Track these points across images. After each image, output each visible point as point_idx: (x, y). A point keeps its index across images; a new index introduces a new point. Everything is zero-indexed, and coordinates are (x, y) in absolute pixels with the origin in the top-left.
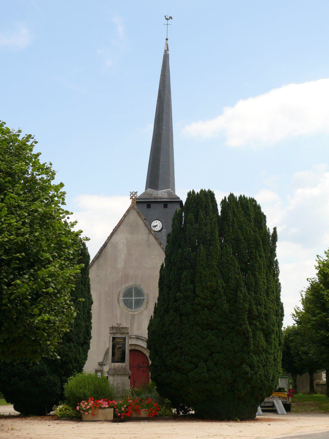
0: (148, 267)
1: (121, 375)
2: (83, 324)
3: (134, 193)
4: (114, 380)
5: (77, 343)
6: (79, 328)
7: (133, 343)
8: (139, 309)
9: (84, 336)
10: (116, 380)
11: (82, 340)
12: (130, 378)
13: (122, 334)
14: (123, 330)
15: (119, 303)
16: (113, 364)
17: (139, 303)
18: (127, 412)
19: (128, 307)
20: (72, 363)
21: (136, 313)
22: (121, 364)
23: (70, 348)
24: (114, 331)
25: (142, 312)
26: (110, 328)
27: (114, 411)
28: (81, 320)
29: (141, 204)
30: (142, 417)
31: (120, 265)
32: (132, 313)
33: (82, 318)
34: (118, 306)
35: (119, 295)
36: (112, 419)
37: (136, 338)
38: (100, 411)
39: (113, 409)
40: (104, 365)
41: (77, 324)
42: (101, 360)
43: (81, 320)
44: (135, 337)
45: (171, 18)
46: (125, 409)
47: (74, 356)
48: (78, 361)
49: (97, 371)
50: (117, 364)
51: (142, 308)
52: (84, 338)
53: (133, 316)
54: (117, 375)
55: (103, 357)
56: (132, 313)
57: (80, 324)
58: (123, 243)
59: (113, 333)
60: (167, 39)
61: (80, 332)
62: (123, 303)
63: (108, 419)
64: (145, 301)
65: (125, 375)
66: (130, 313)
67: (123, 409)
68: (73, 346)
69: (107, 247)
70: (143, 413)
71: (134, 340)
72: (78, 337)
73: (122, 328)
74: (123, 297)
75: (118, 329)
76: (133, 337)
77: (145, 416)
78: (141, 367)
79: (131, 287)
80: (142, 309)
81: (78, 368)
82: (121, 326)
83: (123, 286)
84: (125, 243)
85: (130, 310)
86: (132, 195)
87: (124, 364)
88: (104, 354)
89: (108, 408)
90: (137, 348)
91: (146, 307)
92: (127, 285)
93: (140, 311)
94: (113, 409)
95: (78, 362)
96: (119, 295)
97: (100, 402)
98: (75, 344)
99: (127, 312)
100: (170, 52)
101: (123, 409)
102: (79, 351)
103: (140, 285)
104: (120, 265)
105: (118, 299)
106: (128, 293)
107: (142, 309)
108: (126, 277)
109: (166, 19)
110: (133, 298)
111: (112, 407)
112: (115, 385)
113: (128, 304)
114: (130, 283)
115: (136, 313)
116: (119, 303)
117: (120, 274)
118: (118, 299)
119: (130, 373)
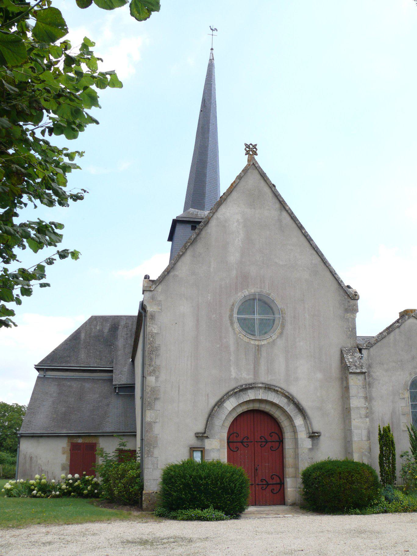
0: (281, 263)
3: (247, 149)
15: (232, 323)
21: (263, 343)
25: (274, 341)
29: (183, 225)
31: (234, 257)
32: (257, 343)
34: (230, 329)
35: (232, 310)
37: (265, 388)
40: (207, 437)
42: (200, 428)
44: (264, 386)
45: (216, 29)
49: (192, 449)
53: (259, 348)
55: (205, 422)
56: (257, 343)
58: (238, 221)
60: (212, 49)
66: (252, 342)
69: (209, 225)
71: (261, 391)
76: (260, 385)
79: (252, 297)
83: (239, 294)
84: (241, 221)
86: (251, 146)
88: (206, 416)
90: (257, 406)
91: (281, 333)
92: (246, 293)
93: (271, 340)
96: (232, 310)
100: (216, 62)
103: (269, 294)
104: (234, 257)
105: (231, 316)
106: (248, 304)
108: (244, 279)
109: (211, 29)
110: (257, 316)
113: (248, 327)
116: (232, 323)
117: (234, 273)
118: (231, 316)
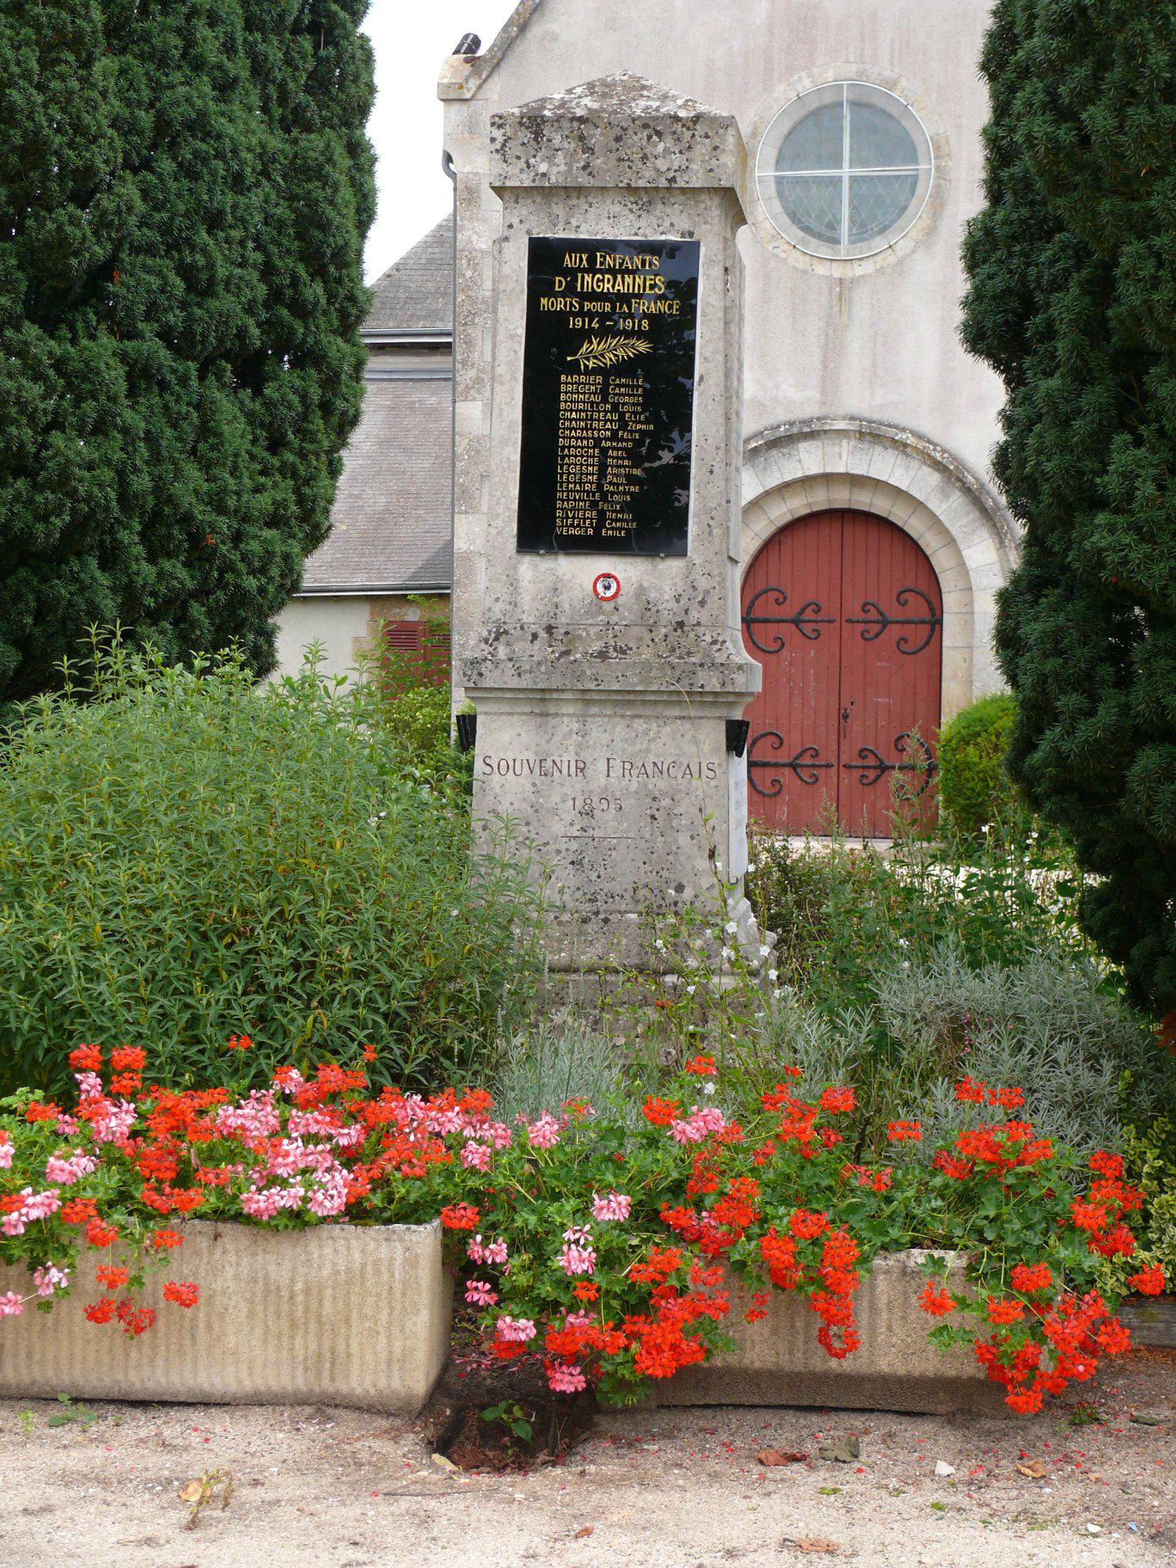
1: (628, 701)
2: (247, 128)
4: (543, 768)
5: (180, 342)
6: (188, 171)
7: (842, 470)
8: (879, 243)
9: (268, 271)
10: (567, 757)
11: (236, 307)
12: (736, 737)
13: (644, 197)
14: (665, 159)
16: (536, 571)
17: (879, 211)
18: (637, 1305)
19: (807, 230)
20: (111, 558)
21: (858, 270)
22: (629, 571)
23: (77, 380)
24: (554, 169)
26: (499, 122)
27: (459, 1267)
28: (225, 87)
30: (887, 1383)
32: (837, 271)
33: (239, 67)
36: (417, 1378)
37: (861, 435)
38: (225, 1268)
39: (424, 1239)
41: (162, 125)
43: (225, 87)
44: (854, 426)
46: (608, 1259)
47: (142, 482)
48: (195, 539)
50: (580, 573)
51: (903, 240)
52: (275, 296)
53: (843, 290)
54: (586, 698)
56: (837, 271)
57: (199, 126)
59: (544, 193)
61: (214, 221)
62: (777, 206)
63: (362, 1380)
64: (925, 189)
65: (684, 700)
66: (821, 269)
67: (576, 1259)
68: (115, 376)
70: (900, 1317)
71: (846, 446)
72: (185, 271)
73: (653, 126)
74: (779, 162)
75: (597, 137)
76: (841, 425)
77: (929, 1362)
78: (885, 623)
79: (828, 99)
80: (904, 247)
81: (197, 610)
82: (638, 108)
85: (825, 251)
87: (673, 566)
89: (356, 1213)
90: (863, 500)
92: (805, 85)
93: (891, 258)
94: (424, 1239)
95: (198, 551)
97: (228, 1116)
98: (152, 346)
99: (802, 262)
101: (576, 1259)
102: (206, 430)
103: (892, 84)
107: (904, 247)
110: (846, 171)
111: (411, 1214)
112: (561, 826)
114: (828, 71)
115: (858, 270)
119: (753, 679)
